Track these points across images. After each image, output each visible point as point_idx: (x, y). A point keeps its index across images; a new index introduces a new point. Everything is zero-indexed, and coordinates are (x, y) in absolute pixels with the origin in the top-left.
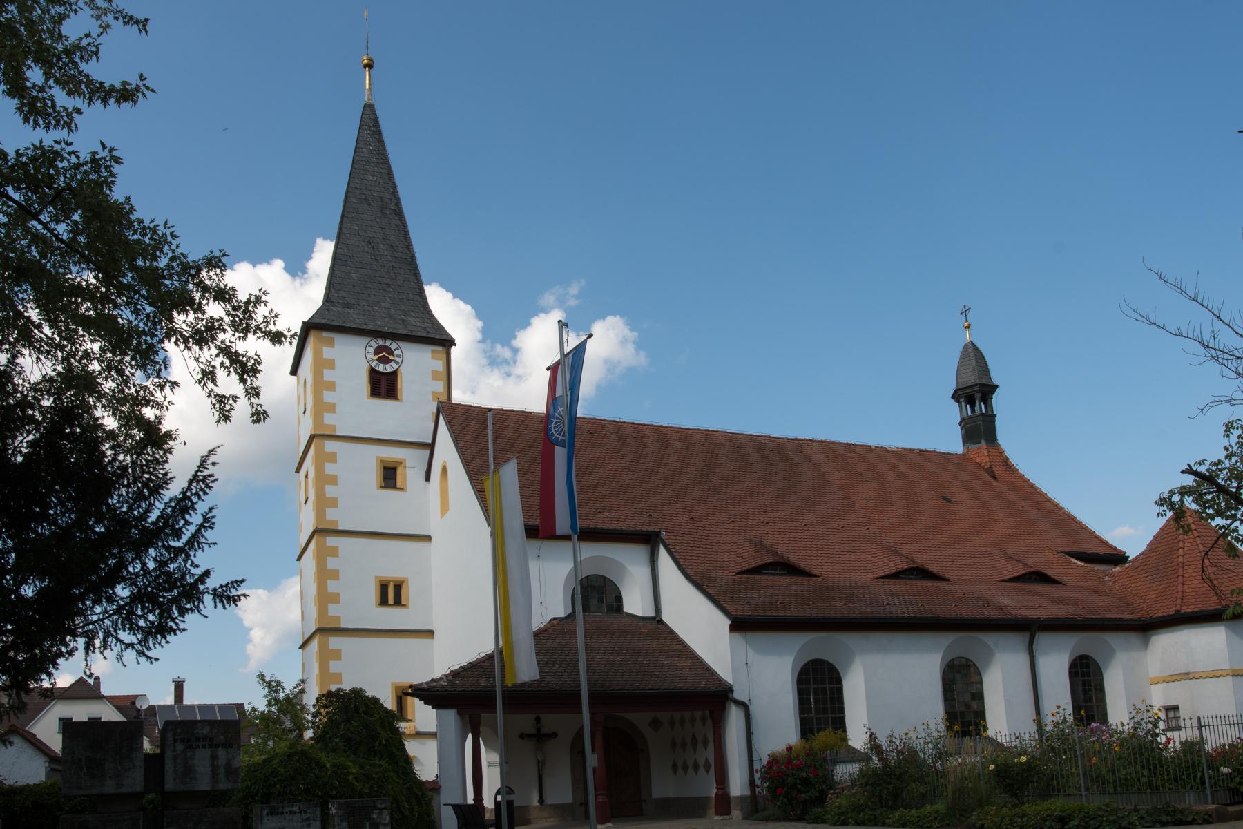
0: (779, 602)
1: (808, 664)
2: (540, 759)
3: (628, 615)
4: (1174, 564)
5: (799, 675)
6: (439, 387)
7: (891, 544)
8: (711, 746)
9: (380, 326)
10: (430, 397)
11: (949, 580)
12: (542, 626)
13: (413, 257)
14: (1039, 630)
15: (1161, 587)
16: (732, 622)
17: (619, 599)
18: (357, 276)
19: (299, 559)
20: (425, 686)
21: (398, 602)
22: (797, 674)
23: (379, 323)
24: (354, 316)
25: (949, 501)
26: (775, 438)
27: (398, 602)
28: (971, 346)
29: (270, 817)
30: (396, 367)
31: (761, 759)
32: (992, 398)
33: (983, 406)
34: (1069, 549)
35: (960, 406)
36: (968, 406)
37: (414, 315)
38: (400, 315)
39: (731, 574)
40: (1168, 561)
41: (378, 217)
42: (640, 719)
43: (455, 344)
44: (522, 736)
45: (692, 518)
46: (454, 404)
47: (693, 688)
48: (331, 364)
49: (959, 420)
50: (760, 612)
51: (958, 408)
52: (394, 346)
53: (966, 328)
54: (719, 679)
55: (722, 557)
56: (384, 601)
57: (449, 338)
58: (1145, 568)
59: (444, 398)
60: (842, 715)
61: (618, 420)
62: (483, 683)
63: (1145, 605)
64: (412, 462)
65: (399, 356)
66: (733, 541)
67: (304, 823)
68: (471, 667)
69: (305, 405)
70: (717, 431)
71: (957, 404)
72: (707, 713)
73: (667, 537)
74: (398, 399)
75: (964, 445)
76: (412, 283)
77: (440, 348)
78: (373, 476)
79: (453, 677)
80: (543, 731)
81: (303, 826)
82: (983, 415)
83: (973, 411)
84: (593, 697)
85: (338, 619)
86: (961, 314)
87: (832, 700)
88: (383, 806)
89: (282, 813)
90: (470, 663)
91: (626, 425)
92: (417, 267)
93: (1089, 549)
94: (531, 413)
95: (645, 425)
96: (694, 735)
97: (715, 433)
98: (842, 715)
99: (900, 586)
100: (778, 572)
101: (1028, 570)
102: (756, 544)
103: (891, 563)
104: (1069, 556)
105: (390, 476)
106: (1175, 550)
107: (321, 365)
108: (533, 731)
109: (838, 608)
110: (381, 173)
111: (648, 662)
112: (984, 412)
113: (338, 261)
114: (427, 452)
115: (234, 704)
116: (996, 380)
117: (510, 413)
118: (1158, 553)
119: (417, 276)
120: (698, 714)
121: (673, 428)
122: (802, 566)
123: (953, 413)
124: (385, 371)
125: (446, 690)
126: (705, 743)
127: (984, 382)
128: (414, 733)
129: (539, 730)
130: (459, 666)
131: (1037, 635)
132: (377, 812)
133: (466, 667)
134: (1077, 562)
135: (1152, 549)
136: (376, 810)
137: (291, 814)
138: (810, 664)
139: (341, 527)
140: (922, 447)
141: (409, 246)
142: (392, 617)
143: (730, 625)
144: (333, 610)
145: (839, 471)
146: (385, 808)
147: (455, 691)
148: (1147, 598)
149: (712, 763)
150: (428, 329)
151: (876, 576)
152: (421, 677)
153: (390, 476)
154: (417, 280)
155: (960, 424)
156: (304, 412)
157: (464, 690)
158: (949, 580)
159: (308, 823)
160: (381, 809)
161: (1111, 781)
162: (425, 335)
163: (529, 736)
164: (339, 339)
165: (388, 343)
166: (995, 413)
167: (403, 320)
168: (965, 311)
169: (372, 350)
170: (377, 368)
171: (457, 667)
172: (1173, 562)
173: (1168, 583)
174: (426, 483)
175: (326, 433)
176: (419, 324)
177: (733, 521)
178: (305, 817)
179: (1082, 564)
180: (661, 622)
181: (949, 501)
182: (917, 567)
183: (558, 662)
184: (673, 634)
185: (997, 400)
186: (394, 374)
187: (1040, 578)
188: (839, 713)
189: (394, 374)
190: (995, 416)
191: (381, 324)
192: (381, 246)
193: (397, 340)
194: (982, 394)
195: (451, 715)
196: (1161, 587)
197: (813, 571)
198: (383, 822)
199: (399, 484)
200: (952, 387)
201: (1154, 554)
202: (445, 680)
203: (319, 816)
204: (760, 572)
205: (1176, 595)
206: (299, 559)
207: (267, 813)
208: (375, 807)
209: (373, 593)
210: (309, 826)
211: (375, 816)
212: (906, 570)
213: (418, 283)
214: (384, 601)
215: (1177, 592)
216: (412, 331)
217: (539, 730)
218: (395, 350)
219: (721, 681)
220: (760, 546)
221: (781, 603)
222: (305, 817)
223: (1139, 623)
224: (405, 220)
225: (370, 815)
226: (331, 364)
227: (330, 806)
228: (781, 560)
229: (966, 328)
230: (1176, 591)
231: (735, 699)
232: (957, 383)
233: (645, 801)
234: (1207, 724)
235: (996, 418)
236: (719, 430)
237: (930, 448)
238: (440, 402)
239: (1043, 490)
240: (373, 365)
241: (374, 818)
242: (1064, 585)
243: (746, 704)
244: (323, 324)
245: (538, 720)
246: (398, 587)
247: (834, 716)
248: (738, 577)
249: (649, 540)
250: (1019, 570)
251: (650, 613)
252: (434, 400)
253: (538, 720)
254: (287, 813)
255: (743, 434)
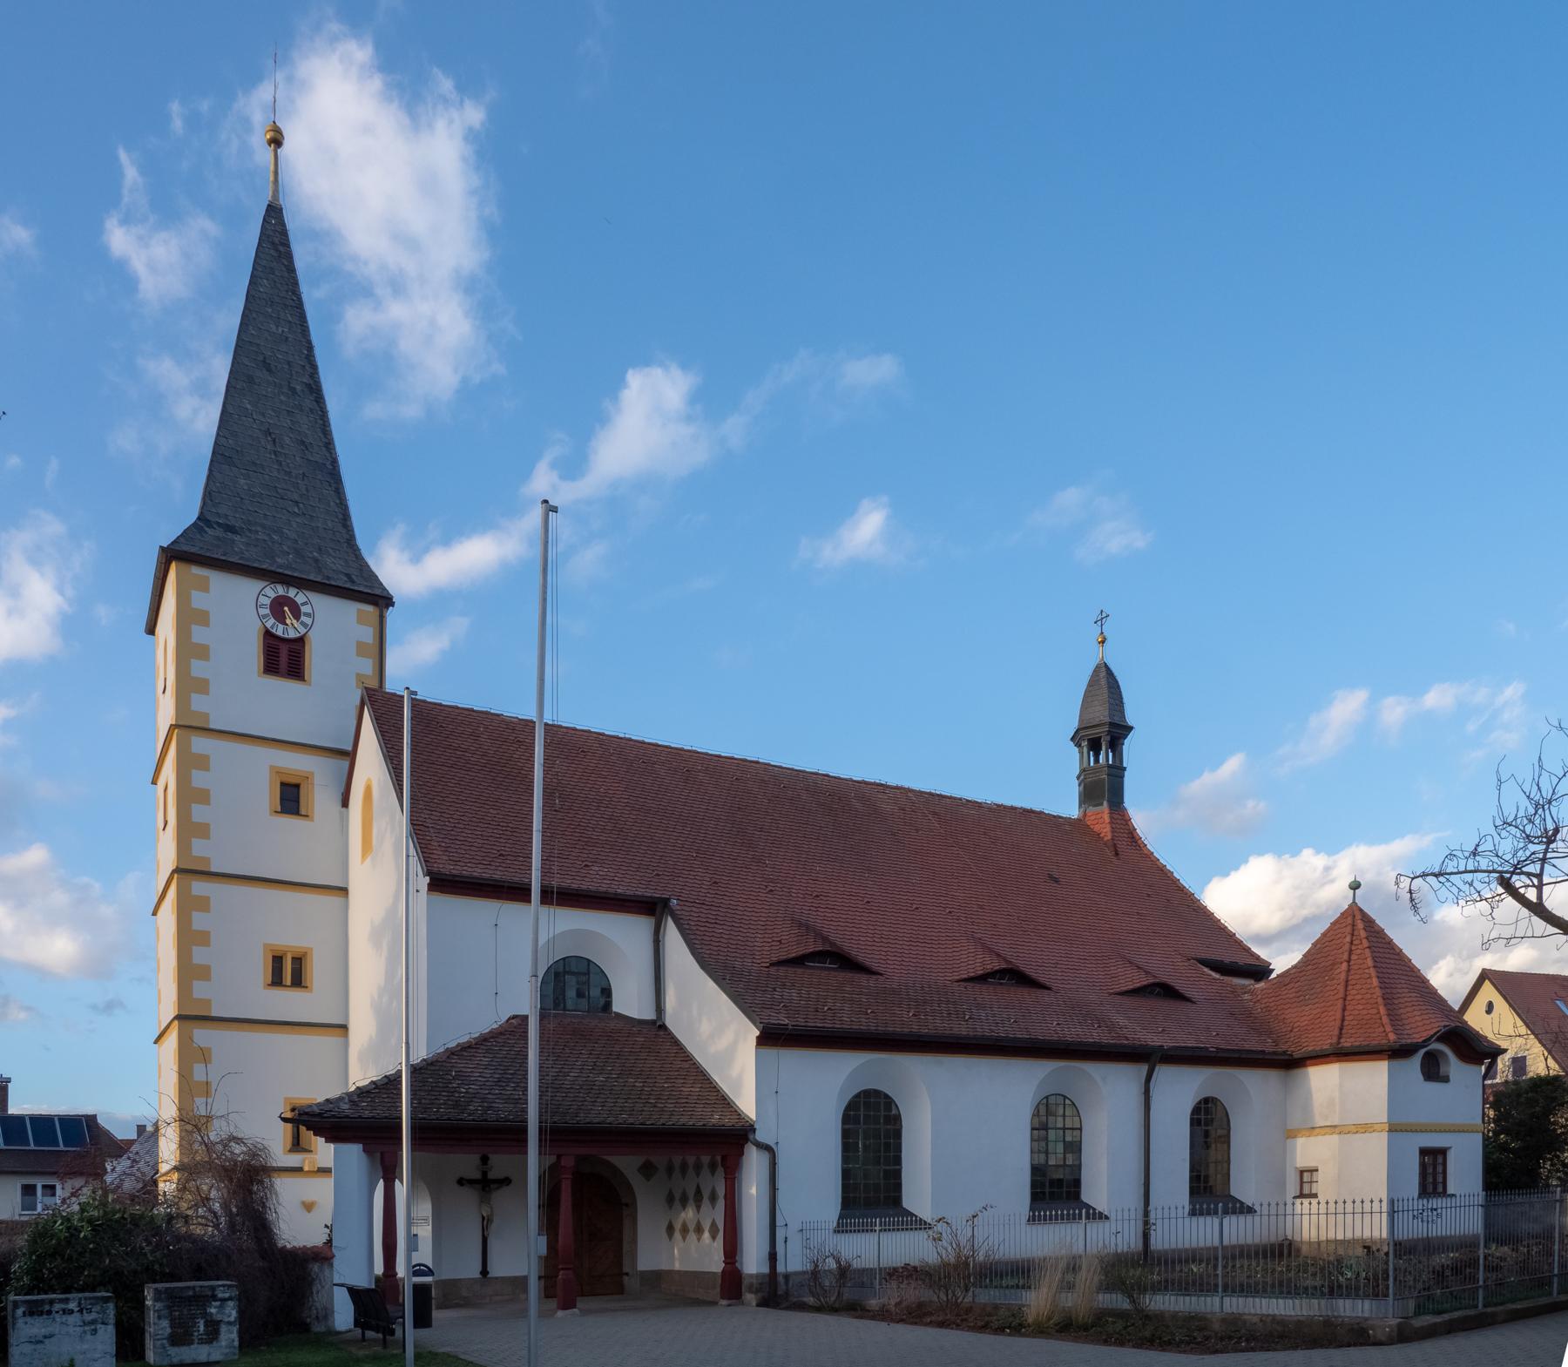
0: (826, 1008)
1: (858, 1096)
2: (485, 1215)
3: (618, 1015)
4: (1335, 981)
5: (845, 1111)
6: (367, 667)
7: (979, 936)
8: (721, 1204)
9: (280, 566)
10: (353, 682)
11: (1049, 989)
12: (495, 1026)
13: (335, 462)
14: (1160, 1062)
15: (1315, 1012)
16: (761, 1033)
17: (607, 992)
18: (247, 484)
19: (155, 913)
20: (317, 1110)
21: (298, 981)
22: (843, 1108)
23: (279, 560)
24: (241, 546)
25: (1056, 881)
26: (835, 778)
27: (298, 981)
28: (1104, 669)
29: (28, 1319)
30: (303, 630)
31: (786, 1225)
32: (1123, 744)
33: (1111, 754)
34: (1203, 956)
35: (1081, 753)
36: (1091, 753)
37: (333, 554)
38: (311, 552)
39: (762, 965)
40: (1327, 978)
41: (283, 393)
42: (626, 1163)
43: (392, 604)
44: (461, 1182)
45: (715, 883)
46: (388, 693)
47: (701, 1124)
48: (203, 618)
49: (1078, 772)
50: (801, 1022)
51: (1078, 755)
52: (300, 598)
53: (1099, 643)
54: (737, 1113)
55: (753, 940)
56: (277, 981)
57: (385, 594)
58: (1297, 985)
59: (374, 684)
60: (897, 1167)
61: (622, 735)
62: (380, 1112)
63: (1292, 1035)
64: (319, 774)
65: (307, 615)
66: (769, 919)
67: (86, 1328)
68: (387, 1083)
69: (165, 679)
70: (757, 762)
71: (1076, 749)
72: (719, 1158)
73: (679, 908)
74: (304, 680)
75: (1080, 806)
76: (332, 504)
77: (369, 608)
78: (265, 795)
79: (359, 1096)
80: (491, 1176)
81: (85, 1332)
82: (1109, 766)
83: (1097, 761)
84: (553, 1135)
85: (208, 1002)
86: (1095, 623)
87: (887, 1145)
88: (227, 1295)
89: (49, 1313)
90: (386, 1076)
91: (631, 743)
92: (341, 480)
93: (1227, 957)
94: (498, 715)
95: (659, 746)
96: (698, 1187)
97: (754, 765)
98: (897, 1167)
99: (985, 993)
100: (827, 965)
101: (1152, 980)
102: (800, 925)
103: (978, 961)
104: (1201, 963)
105: (291, 798)
106: (1338, 963)
107: (188, 618)
108: (477, 1175)
109: (905, 1021)
110: (290, 322)
111: (641, 1084)
112: (1110, 763)
113: (219, 456)
114: (346, 764)
115: (82, 1116)
116: (1131, 718)
117: (467, 713)
118: (1316, 966)
119: (339, 493)
120: (706, 1159)
121: (698, 753)
122: (860, 959)
123: (1071, 761)
124: (286, 636)
125: (347, 1117)
126: (713, 1198)
127: (1117, 720)
128: (316, 1169)
129: (485, 1174)
130: (369, 1080)
131: (1157, 1068)
132: (218, 1303)
133: (379, 1084)
134: (1213, 974)
135: (1308, 960)
136: (215, 1301)
137: (64, 1313)
138: (862, 1096)
139: (213, 869)
140: (1027, 805)
141: (329, 444)
142: (288, 1003)
143: (758, 1037)
144: (200, 989)
145: (917, 831)
146: (230, 1299)
147: (360, 1117)
148: (1296, 1025)
149: (721, 1226)
150: (353, 577)
151: (958, 978)
152: (319, 1091)
153: (291, 798)
154: (340, 499)
155: (1078, 778)
156: (164, 692)
157: (373, 1117)
158: (1049, 989)
159: (93, 1327)
160: (224, 1300)
161: (1239, 1271)
162: (348, 585)
163: (471, 1182)
164: (217, 580)
165: (292, 592)
166: (1125, 765)
167: (316, 561)
168: (1102, 619)
169: (267, 601)
170: (274, 631)
171: (366, 1082)
172: (1333, 979)
173: (1325, 1006)
174: (344, 809)
175: (194, 724)
176: (340, 567)
177: (771, 891)
178: (88, 1317)
179: (1217, 976)
180: (663, 1027)
181: (1056, 881)
182: (1011, 969)
183: (515, 1080)
184: (678, 1045)
185: (1130, 746)
186: (301, 640)
187: (1166, 991)
188: (895, 1165)
189: (301, 640)
190: (1125, 769)
191: (281, 563)
192: (287, 440)
193: (307, 589)
194: (1112, 737)
195: (354, 1151)
196: (1315, 1012)
197: (874, 966)
198: (226, 1320)
199: (303, 811)
200: (1074, 725)
201: (1310, 967)
202: (346, 1100)
203: (112, 1316)
204: (804, 964)
205: (1333, 1023)
206: (155, 913)
207: (24, 1313)
208: (214, 1298)
209: (262, 970)
210: (95, 1332)
211: (213, 1310)
212: (997, 972)
213: (341, 504)
214: (277, 981)
215: (1335, 1020)
216: (328, 578)
217: (485, 1174)
218: (303, 604)
219: (740, 1115)
220: (805, 928)
221: (829, 1009)
222: (88, 1317)
223: (1283, 1057)
224: (324, 403)
225: (205, 1309)
226: (203, 618)
227: (146, 1293)
228: (834, 949)
229: (1099, 643)
230: (1334, 1018)
231: (757, 1141)
232: (1081, 720)
233: (627, 1274)
234: (1401, 1209)
235: (1126, 773)
236: (761, 761)
237: (1037, 808)
238: (366, 688)
239: (1175, 875)
240: (269, 625)
241: (212, 1314)
242: (1194, 1003)
243: (771, 1147)
244: (192, 553)
245: (485, 1160)
246: (299, 961)
247: (888, 1168)
248: (773, 970)
249: (652, 908)
250: (1141, 980)
251: (648, 1014)
252: (357, 687)
253: (485, 1160)
254: (57, 1312)
255: (792, 769)
